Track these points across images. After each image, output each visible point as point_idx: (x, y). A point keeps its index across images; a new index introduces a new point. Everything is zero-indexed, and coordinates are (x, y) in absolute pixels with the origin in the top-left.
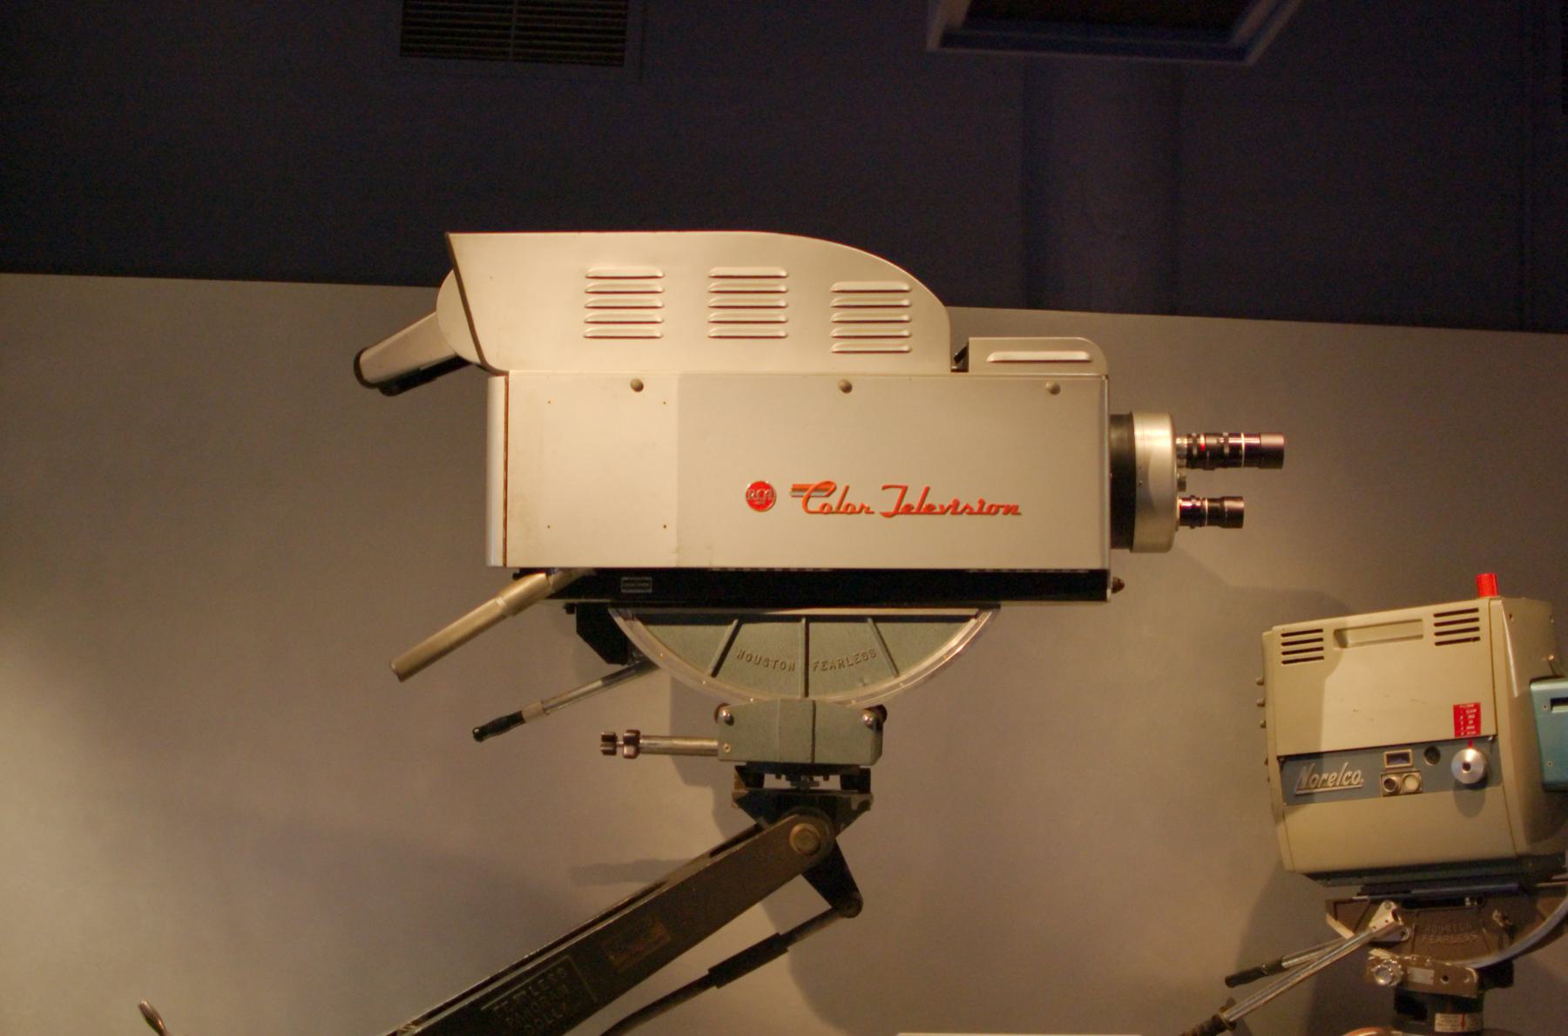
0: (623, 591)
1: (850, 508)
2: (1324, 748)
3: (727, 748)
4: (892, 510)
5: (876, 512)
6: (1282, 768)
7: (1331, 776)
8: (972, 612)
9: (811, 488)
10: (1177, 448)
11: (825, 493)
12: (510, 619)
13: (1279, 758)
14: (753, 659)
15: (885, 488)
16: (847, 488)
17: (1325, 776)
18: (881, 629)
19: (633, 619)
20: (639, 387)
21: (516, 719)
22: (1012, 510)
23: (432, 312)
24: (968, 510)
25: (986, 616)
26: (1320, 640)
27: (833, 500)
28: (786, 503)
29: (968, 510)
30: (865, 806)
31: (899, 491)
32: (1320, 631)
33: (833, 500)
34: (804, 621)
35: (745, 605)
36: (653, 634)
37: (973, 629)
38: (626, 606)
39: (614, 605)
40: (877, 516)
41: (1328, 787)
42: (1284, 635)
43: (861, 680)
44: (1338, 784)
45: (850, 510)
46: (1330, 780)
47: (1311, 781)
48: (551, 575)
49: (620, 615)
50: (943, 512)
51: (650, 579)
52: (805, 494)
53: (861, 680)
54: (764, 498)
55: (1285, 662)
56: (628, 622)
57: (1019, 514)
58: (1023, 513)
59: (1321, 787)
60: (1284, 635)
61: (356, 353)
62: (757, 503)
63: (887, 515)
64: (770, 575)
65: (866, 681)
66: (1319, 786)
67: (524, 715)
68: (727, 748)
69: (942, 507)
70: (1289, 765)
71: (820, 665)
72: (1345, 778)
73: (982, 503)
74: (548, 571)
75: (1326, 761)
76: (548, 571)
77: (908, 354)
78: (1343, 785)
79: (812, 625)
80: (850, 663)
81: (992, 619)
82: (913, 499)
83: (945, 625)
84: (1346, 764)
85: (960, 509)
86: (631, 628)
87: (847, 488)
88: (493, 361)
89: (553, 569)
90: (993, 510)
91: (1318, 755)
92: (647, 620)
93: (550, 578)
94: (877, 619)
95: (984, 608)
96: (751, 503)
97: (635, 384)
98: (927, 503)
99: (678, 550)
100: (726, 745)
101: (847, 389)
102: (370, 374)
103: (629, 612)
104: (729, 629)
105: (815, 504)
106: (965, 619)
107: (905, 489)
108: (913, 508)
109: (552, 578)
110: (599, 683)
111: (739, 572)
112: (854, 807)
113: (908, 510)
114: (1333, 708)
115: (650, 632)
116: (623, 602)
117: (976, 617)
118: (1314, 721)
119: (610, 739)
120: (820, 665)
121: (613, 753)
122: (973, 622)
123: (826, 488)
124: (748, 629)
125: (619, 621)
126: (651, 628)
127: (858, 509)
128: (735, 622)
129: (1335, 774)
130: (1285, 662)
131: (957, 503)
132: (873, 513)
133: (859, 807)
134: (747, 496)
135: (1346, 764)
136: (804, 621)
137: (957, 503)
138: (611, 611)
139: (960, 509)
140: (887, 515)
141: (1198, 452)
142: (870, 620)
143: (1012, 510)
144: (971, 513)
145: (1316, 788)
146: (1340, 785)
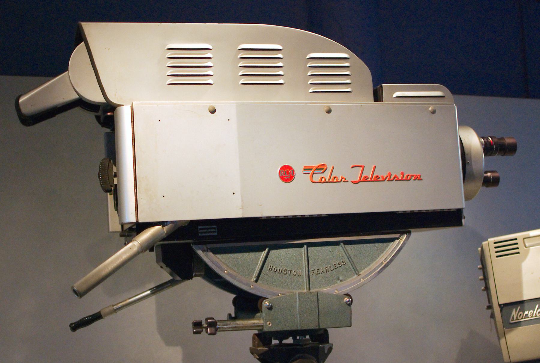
0: (200, 235)
1: (323, 179)
2: (525, 298)
3: (269, 324)
4: (358, 180)
5: (349, 181)
6: (501, 311)
7: (530, 312)
8: (397, 236)
9: (314, 168)
10: (481, 143)
11: (322, 171)
12: (141, 254)
13: (500, 305)
14: (278, 270)
15: (352, 168)
16: (333, 168)
17: (526, 313)
18: (348, 249)
19: (207, 251)
20: (213, 111)
21: (97, 317)
22: (418, 178)
23: (66, 71)
24: (396, 178)
25: (405, 237)
26: (517, 244)
27: (327, 175)
28: (300, 177)
29: (396, 178)
30: (330, 349)
31: (361, 169)
32: (516, 239)
33: (327, 175)
34: (306, 246)
35: (273, 239)
36: (219, 259)
37: (397, 245)
38: (205, 243)
39: (195, 243)
40: (350, 183)
41: (529, 318)
42: (495, 243)
43: (338, 279)
44: (534, 316)
45: (334, 181)
46: (529, 314)
47: (518, 316)
48: (165, 226)
49: (200, 249)
50: (384, 180)
51: (215, 226)
52: (311, 172)
53: (338, 279)
54: (289, 175)
55: (497, 257)
56: (205, 253)
57: (421, 180)
58: (423, 179)
59: (525, 318)
60: (495, 243)
61: (17, 95)
62: (285, 178)
63: (355, 183)
64: (303, 219)
65: (341, 278)
66: (524, 318)
67: (102, 313)
68: (269, 324)
69: (383, 177)
70: (505, 309)
71: (316, 272)
72: (537, 313)
73: (403, 174)
74: (163, 224)
75: (526, 304)
76: (163, 224)
77: (351, 93)
78: (537, 316)
79: (310, 249)
80: (332, 269)
81: (407, 239)
82: (368, 173)
83: (381, 244)
84: (537, 306)
85: (392, 178)
86: (207, 256)
87: (333, 168)
88: (114, 99)
89: (167, 222)
90: (408, 179)
91: (521, 303)
92: (216, 252)
93: (164, 228)
94: (346, 243)
95: (402, 233)
96: (282, 178)
97: (211, 109)
98: (375, 175)
99: (242, 208)
100: (268, 323)
101: (329, 111)
102: (27, 110)
103: (205, 247)
104: (263, 254)
105: (317, 178)
106: (393, 240)
107: (363, 167)
108: (368, 178)
109: (166, 228)
110: (149, 292)
111: (435, 212)
112: (326, 351)
113: (366, 179)
114: (526, 277)
115: (218, 258)
116: (203, 242)
117: (398, 239)
118: (519, 285)
119: (197, 325)
120: (316, 272)
121: (199, 333)
122: (397, 241)
123: (322, 168)
124: (274, 253)
125: (200, 252)
126: (218, 256)
127: (340, 180)
128: (267, 250)
129: (531, 311)
130: (497, 257)
131: (390, 175)
132: (347, 181)
133: (328, 351)
134: (279, 174)
135: (537, 306)
136: (306, 246)
137: (390, 175)
138: (194, 247)
139: (392, 178)
140: (355, 183)
141: (494, 143)
142: (342, 244)
143: (418, 178)
144: (398, 180)
145: (522, 318)
146: (535, 316)
